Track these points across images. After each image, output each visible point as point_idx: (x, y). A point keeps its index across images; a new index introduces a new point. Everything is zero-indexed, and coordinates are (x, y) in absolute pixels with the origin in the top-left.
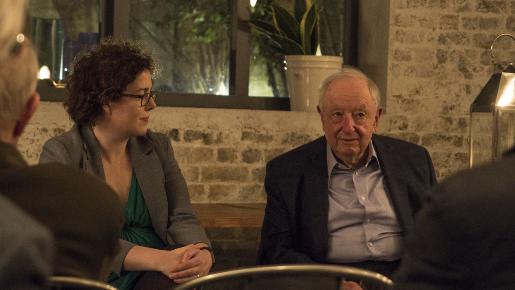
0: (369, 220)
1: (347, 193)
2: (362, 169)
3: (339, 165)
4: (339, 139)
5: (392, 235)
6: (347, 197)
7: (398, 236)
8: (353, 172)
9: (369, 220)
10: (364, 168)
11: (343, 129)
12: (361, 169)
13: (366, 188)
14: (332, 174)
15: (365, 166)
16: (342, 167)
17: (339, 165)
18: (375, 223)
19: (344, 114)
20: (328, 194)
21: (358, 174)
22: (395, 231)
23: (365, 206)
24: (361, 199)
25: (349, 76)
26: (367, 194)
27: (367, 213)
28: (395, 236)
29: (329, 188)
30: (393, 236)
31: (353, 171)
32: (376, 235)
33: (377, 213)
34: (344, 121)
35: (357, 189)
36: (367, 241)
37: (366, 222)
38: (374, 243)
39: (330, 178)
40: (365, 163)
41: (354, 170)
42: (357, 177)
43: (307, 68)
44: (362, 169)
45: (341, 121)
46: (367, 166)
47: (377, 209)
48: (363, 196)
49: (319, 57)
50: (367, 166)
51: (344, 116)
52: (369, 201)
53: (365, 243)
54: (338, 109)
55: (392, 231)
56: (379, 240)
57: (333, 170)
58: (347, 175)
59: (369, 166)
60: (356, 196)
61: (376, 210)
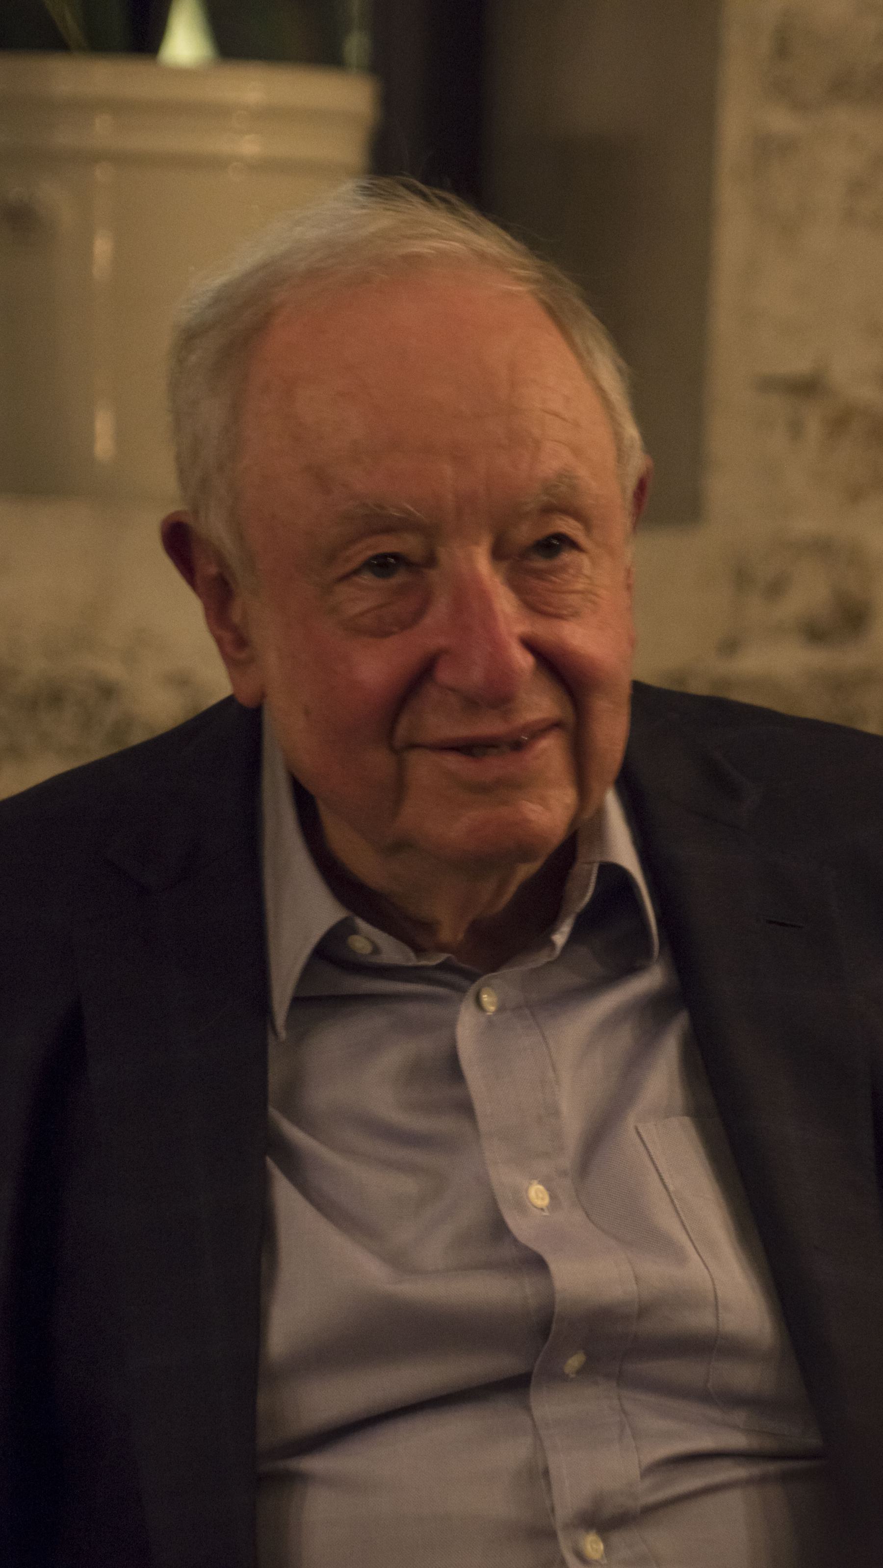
0: (574, 1362)
1: (417, 1156)
2: (532, 965)
3: (354, 931)
4: (413, 746)
5: (739, 1472)
6: (408, 1185)
7: (785, 1478)
8: (462, 991)
9: (574, 1362)
10: (542, 958)
11: (445, 675)
12: (512, 972)
13: (556, 1113)
14: (298, 1001)
15: (552, 944)
16: (376, 950)
17: (354, 931)
18: (623, 1380)
19: (431, 561)
20: (270, 1162)
21: (501, 1009)
22: (769, 1444)
23: (549, 1258)
24: (522, 1205)
25: (419, 256)
26: (567, 1160)
27: (558, 1297)
28: (762, 1481)
29: (273, 1112)
30: (762, 1481)
31: (464, 983)
32: (636, 1472)
33: (644, 1310)
34: (441, 607)
35: (483, 1125)
36: (558, 1525)
37: (557, 1377)
38: (617, 1538)
39: (283, 1034)
40: (551, 923)
41: (472, 977)
42: (491, 1024)
43: (94, 158)
44: (532, 965)
45: (419, 614)
46: (560, 938)
47: (637, 1278)
48: (533, 1177)
49: (181, 73)
50: (560, 938)
51: (433, 575)
52: (578, 1216)
53: (551, 1535)
54: (389, 529)
55: (737, 1441)
56: (651, 1510)
57: (308, 970)
58: (412, 1009)
59: (573, 938)
60: (484, 1182)
61: (632, 1287)
